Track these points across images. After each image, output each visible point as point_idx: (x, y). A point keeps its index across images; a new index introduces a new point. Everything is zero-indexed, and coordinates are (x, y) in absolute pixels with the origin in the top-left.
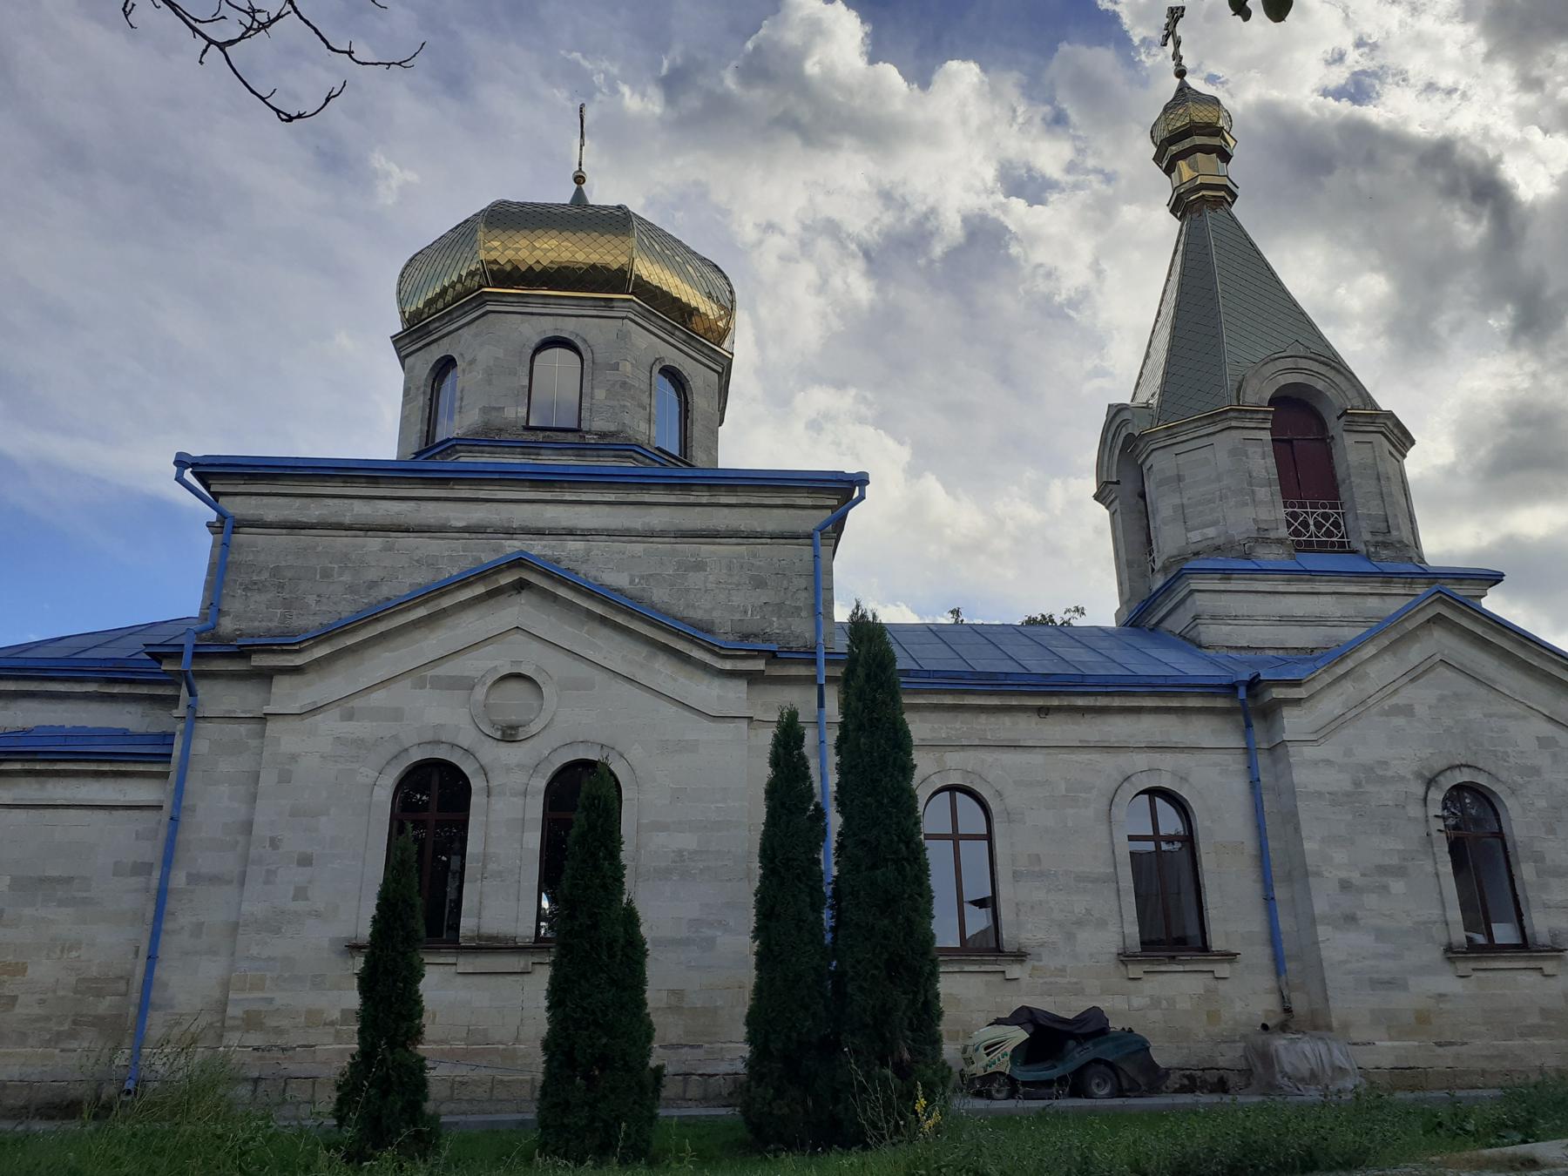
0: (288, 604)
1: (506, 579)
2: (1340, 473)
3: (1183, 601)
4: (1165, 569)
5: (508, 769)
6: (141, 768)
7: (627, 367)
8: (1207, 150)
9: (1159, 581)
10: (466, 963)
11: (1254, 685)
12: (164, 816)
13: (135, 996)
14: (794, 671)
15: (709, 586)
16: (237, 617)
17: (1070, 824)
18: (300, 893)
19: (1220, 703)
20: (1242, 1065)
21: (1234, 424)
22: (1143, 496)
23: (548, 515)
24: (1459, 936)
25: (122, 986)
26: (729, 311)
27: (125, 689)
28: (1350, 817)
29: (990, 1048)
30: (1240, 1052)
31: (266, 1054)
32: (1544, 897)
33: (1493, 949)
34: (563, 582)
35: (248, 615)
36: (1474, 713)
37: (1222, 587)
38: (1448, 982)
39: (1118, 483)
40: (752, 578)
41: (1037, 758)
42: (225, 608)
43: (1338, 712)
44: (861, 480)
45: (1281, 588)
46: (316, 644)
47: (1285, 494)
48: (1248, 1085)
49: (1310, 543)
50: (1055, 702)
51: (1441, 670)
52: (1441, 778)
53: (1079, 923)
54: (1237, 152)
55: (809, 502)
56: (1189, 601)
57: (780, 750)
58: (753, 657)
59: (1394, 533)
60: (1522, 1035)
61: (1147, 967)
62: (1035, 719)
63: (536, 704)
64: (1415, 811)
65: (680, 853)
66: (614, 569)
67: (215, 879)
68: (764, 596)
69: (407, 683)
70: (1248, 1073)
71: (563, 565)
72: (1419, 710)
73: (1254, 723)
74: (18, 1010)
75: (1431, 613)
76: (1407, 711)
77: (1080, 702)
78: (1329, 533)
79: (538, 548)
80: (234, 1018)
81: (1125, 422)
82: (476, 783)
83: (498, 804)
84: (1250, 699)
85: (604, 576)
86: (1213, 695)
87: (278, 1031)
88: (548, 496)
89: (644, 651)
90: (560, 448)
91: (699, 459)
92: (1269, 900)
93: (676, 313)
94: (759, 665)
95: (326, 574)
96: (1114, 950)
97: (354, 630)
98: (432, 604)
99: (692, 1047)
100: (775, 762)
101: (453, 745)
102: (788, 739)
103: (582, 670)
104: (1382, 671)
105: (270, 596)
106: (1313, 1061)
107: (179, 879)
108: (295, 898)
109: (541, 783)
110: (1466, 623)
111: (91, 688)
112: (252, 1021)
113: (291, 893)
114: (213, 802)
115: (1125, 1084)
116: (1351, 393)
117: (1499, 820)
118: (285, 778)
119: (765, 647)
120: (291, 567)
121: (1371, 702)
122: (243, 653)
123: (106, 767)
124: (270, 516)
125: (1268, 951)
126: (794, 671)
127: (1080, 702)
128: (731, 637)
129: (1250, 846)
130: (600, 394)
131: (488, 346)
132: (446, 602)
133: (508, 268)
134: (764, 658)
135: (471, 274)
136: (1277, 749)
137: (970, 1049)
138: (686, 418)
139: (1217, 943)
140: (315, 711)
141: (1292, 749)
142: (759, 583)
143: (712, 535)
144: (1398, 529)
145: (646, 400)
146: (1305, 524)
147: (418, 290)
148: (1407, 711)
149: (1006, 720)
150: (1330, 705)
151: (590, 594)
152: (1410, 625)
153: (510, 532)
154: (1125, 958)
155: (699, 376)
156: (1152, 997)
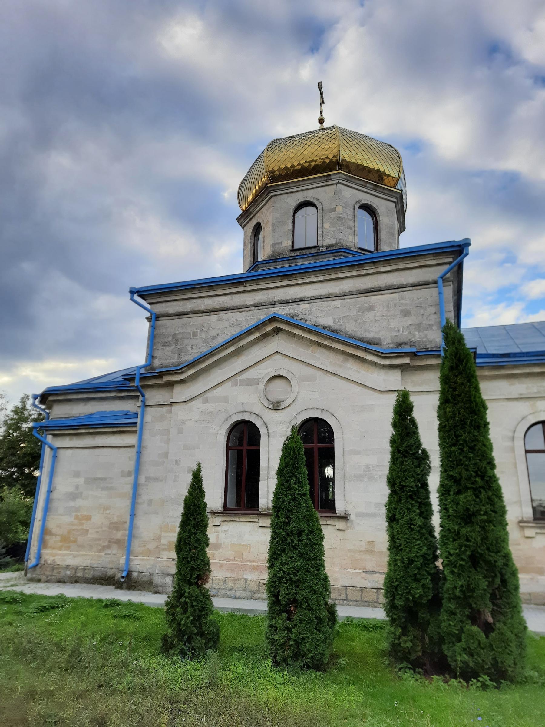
1: (269, 328)
6: (128, 429)
7: (340, 209)
12: (134, 450)
15: (377, 318)
23: (292, 292)
26: (401, 169)
27: (126, 394)
34: (296, 326)
35: (166, 358)
40: (402, 311)
42: (155, 355)
44: (466, 244)
46: (189, 369)
55: (434, 262)
65: (367, 466)
66: (324, 315)
67: (156, 479)
69: (228, 384)
74: (89, 536)
80: (164, 545)
82: (263, 431)
85: (320, 320)
88: (290, 283)
89: (341, 358)
93: (375, 179)
94: (407, 361)
97: (204, 361)
98: (236, 345)
101: (251, 413)
102: (404, 410)
105: (173, 347)
107: (142, 479)
111: (114, 394)
114: (153, 443)
120: (180, 333)
122: (160, 375)
123: (115, 430)
128: (391, 346)
130: (327, 226)
132: (242, 343)
134: (407, 357)
138: (377, 229)
139: (340, 507)
140: (191, 400)
142: (406, 313)
151: (310, 331)
153: (273, 304)
155: (385, 207)
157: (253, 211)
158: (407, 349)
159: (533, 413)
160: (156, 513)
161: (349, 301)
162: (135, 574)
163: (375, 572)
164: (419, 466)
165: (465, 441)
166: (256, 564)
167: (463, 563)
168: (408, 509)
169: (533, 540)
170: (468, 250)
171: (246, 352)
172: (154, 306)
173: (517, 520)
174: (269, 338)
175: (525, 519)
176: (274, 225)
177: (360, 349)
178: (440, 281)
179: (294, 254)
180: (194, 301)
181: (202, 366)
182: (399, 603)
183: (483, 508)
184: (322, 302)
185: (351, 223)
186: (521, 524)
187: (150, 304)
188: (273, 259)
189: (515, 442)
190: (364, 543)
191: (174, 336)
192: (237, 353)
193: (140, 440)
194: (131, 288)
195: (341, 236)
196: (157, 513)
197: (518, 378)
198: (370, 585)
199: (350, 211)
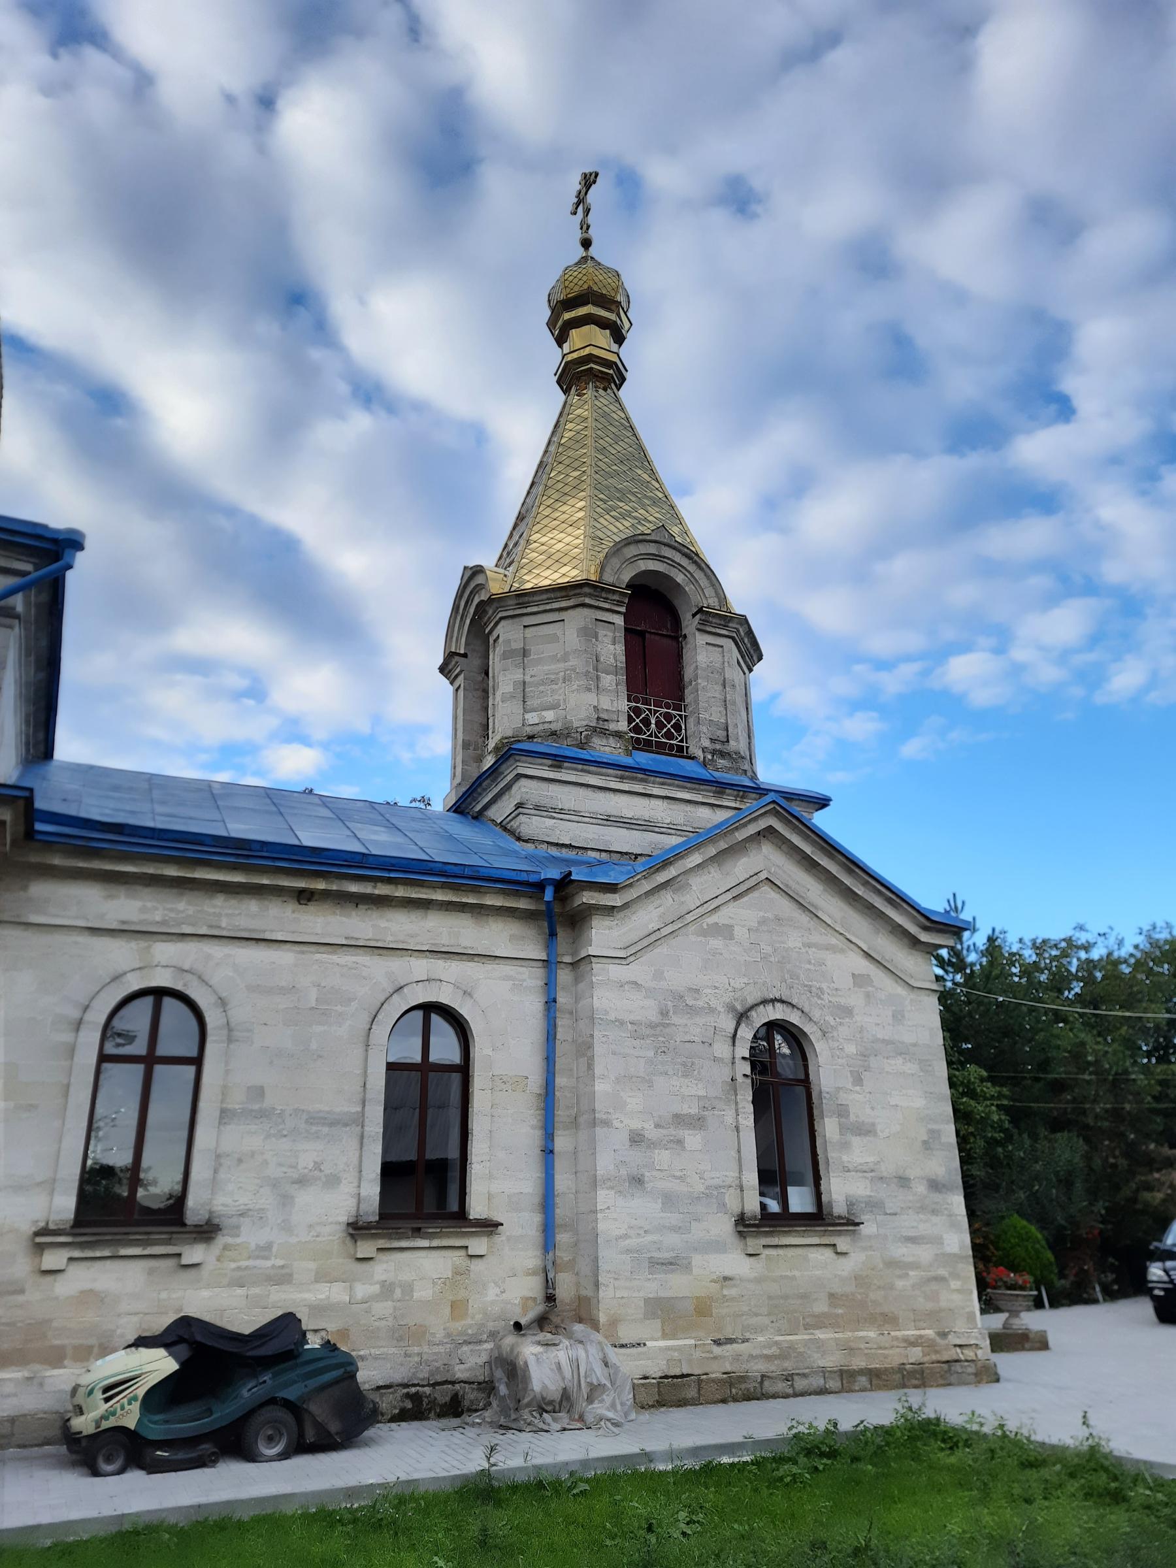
2: (688, 673)
3: (508, 787)
4: (497, 749)
8: (603, 324)
11: (564, 885)
17: (314, 1046)
19: (523, 904)
21: (587, 601)
24: (752, 1204)
28: (651, 1054)
29: (111, 1390)
30: (484, 1358)
32: (845, 1158)
33: (785, 1220)
36: (794, 941)
37: (552, 775)
38: (733, 1261)
39: (465, 655)
41: (285, 957)
43: (654, 926)
45: (613, 785)
49: (648, 743)
50: (321, 885)
51: (766, 889)
52: (753, 1013)
59: (732, 742)
60: (807, 1327)
61: (382, 1243)
64: (722, 1049)
70: (487, 1387)
72: (740, 932)
76: (726, 932)
77: (354, 888)
84: (558, 904)
86: (516, 894)
92: (548, 1152)
96: (344, 1219)
104: (708, 884)
115: (310, 1437)
116: (709, 592)
117: (806, 1067)
121: (689, 918)
125: (537, 1218)
127: (354, 888)
129: (535, 1082)
136: (579, 964)
137: (81, 1391)
139: (477, 1208)
141: (597, 966)
144: (737, 740)
148: (726, 932)
149: (252, 905)
150: (647, 917)
152: (741, 835)
154: (357, 1229)
156: (383, 1283)
159: (140, 968)
169: (59, 1277)
170: (74, 557)
173: (34, 1229)
175: (52, 1226)
186: (39, 1240)
189: (81, 1034)
197: (126, 883)
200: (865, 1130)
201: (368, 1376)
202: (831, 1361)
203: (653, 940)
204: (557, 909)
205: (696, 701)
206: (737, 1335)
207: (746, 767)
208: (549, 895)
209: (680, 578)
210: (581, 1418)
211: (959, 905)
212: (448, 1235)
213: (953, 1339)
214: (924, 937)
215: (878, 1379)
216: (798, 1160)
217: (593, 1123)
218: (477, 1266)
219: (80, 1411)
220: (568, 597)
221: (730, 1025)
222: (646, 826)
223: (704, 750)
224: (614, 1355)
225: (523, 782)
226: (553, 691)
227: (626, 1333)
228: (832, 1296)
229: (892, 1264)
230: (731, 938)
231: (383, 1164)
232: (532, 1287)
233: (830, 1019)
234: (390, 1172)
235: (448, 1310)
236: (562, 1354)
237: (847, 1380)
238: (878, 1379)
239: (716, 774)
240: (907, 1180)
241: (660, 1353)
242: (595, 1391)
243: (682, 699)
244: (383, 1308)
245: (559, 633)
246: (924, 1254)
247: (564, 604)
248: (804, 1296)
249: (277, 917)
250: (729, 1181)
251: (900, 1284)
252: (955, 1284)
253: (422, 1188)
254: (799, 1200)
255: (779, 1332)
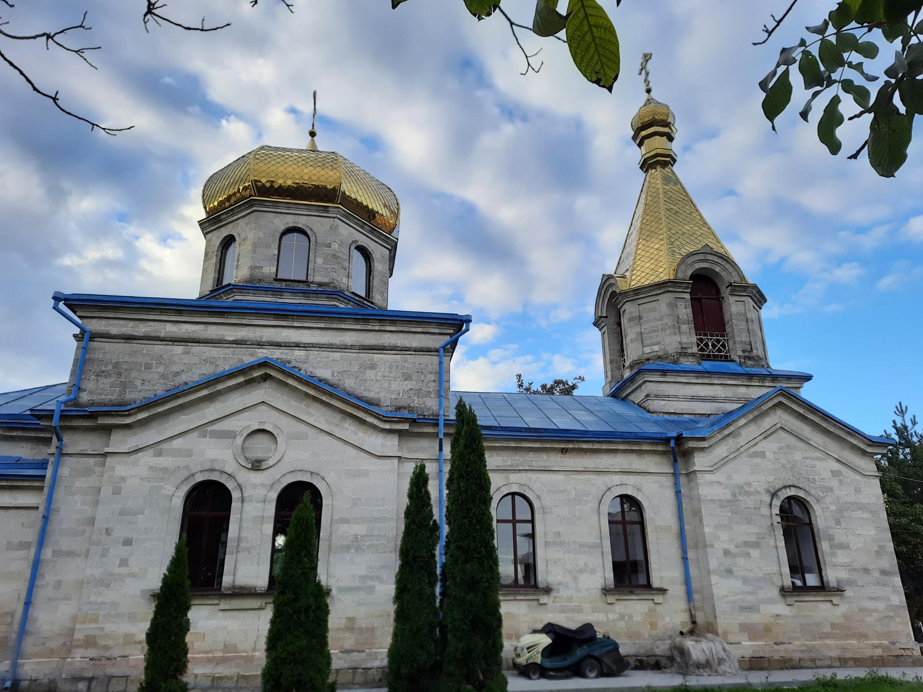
0: (124, 386)
1: (257, 374)
3: (640, 386)
4: (631, 367)
5: (255, 486)
6: (27, 484)
7: (335, 246)
8: (661, 134)
9: (627, 374)
10: (225, 604)
11: (679, 439)
12: (37, 516)
13: (16, 627)
14: (425, 430)
15: (378, 378)
16: (91, 393)
18: (124, 563)
19: (660, 448)
20: (668, 653)
22: (619, 324)
24: (788, 582)
25: (9, 619)
26: (396, 215)
27: (20, 434)
30: (667, 646)
31: (98, 662)
32: (834, 560)
33: (805, 589)
34: (291, 376)
35: (97, 391)
36: (798, 456)
37: (662, 379)
39: (606, 317)
40: (403, 374)
41: (560, 477)
42: (83, 387)
44: (467, 320)
45: (693, 381)
47: (697, 328)
48: (672, 666)
49: (709, 356)
50: (571, 446)
51: (780, 432)
53: (581, 571)
54: (677, 136)
55: (437, 331)
56: (643, 387)
57: (415, 489)
58: (402, 422)
59: (755, 351)
60: (820, 638)
61: (617, 597)
62: (560, 455)
63: (273, 447)
64: (765, 511)
65: (356, 536)
66: (323, 367)
67: (71, 554)
68: (409, 385)
69: (196, 434)
70: (671, 659)
71: (293, 364)
72: (769, 454)
73: (678, 459)
75: (776, 401)
76: (762, 455)
77: (584, 446)
78: (719, 350)
79: (276, 354)
80: (79, 640)
81: (611, 285)
82: (235, 495)
83: (248, 507)
84: (677, 447)
86: (657, 444)
87: (106, 648)
89: (339, 416)
90: (295, 292)
91: (377, 298)
92: (685, 559)
93: (363, 215)
94: (406, 427)
95: (148, 367)
96: (600, 587)
99: (359, 651)
100: (411, 496)
102: (419, 480)
103: (303, 428)
104: (750, 432)
106: (708, 653)
107: (47, 553)
108: (120, 565)
109: (274, 495)
110: (794, 407)
112: (90, 642)
113: (118, 563)
114: (71, 505)
115: (605, 670)
116: (734, 274)
118: (117, 491)
119: (410, 416)
120: (127, 362)
121: (743, 449)
124: (114, 331)
126: (425, 430)
127: (584, 446)
128: (390, 409)
129: (675, 527)
130: (320, 261)
131: (255, 233)
132: (220, 387)
133: (268, 185)
134: (409, 424)
135: (245, 188)
136: (690, 474)
137: (519, 649)
138: (370, 274)
139: (656, 583)
141: (699, 475)
142: (407, 377)
143: (381, 349)
144: (757, 349)
145: (346, 264)
146: (707, 345)
147: (214, 197)
148: (762, 455)
149: (544, 456)
150: (721, 451)
151: (307, 383)
152: (764, 408)
153: (261, 344)
154: (606, 591)
155: (378, 252)
156: (620, 614)
157: (225, 219)
158: (406, 414)
160: (67, 598)
161: (351, 355)
162: (25, 684)
163: (352, 651)
164: (431, 537)
165: (474, 514)
166: (211, 655)
167: (465, 627)
168: (419, 579)
171: (222, 398)
172: (85, 321)
174: (254, 384)
176: (255, 245)
177: (358, 408)
178: (442, 350)
179: (277, 285)
180: (152, 324)
181: (160, 409)
182: (405, 671)
183: (485, 576)
184: (320, 350)
185: (346, 264)
187: (80, 317)
188: (252, 285)
190: (344, 621)
191: (116, 365)
192: (211, 398)
193: (50, 500)
194: (56, 292)
195: (335, 276)
196: (69, 599)
198: (346, 666)
199: (346, 251)
200: (844, 547)
201: (623, 651)
202: (835, 653)
203: (725, 461)
204: (676, 449)
205: (733, 332)
206: (786, 640)
207: (764, 363)
208: (672, 444)
209: (717, 269)
210: (716, 672)
211: (904, 409)
212: (645, 594)
213: (898, 646)
214: (869, 450)
215: (858, 662)
216: (809, 560)
217: (705, 546)
218: (658, 608)
219: (518, 656)
220: (660, 288)
221: (768, 499)
222: (713, 400)
223: (739, 357)
224: (727, 647)
225: (648, 384)
226: (657, 336)
227: (731, 638)
228: (832, 624)
229: (863, 610)
230: (765, 457)
231: (614, 563)
232: (685, 617)
233: (821, 494)
234: (617, 566)
235: (649, 626)
236: (704, 645)
237: (843, 662)
238: (858, 662)
239: (747, 369)
240: (868, 570)
241: (748, 647)
242: (721, 661)
243: (724, 330)
244: (621, 624)
245: (657, 306)
246: (881, 605)
247: (658, 292)
248: (819, 624)
249: (555, 460)
250: (775, 571)
251: (868, 619)
252: (898, 620)
253: (630, 574)
254: (812, 580)
255: (806, 640)
